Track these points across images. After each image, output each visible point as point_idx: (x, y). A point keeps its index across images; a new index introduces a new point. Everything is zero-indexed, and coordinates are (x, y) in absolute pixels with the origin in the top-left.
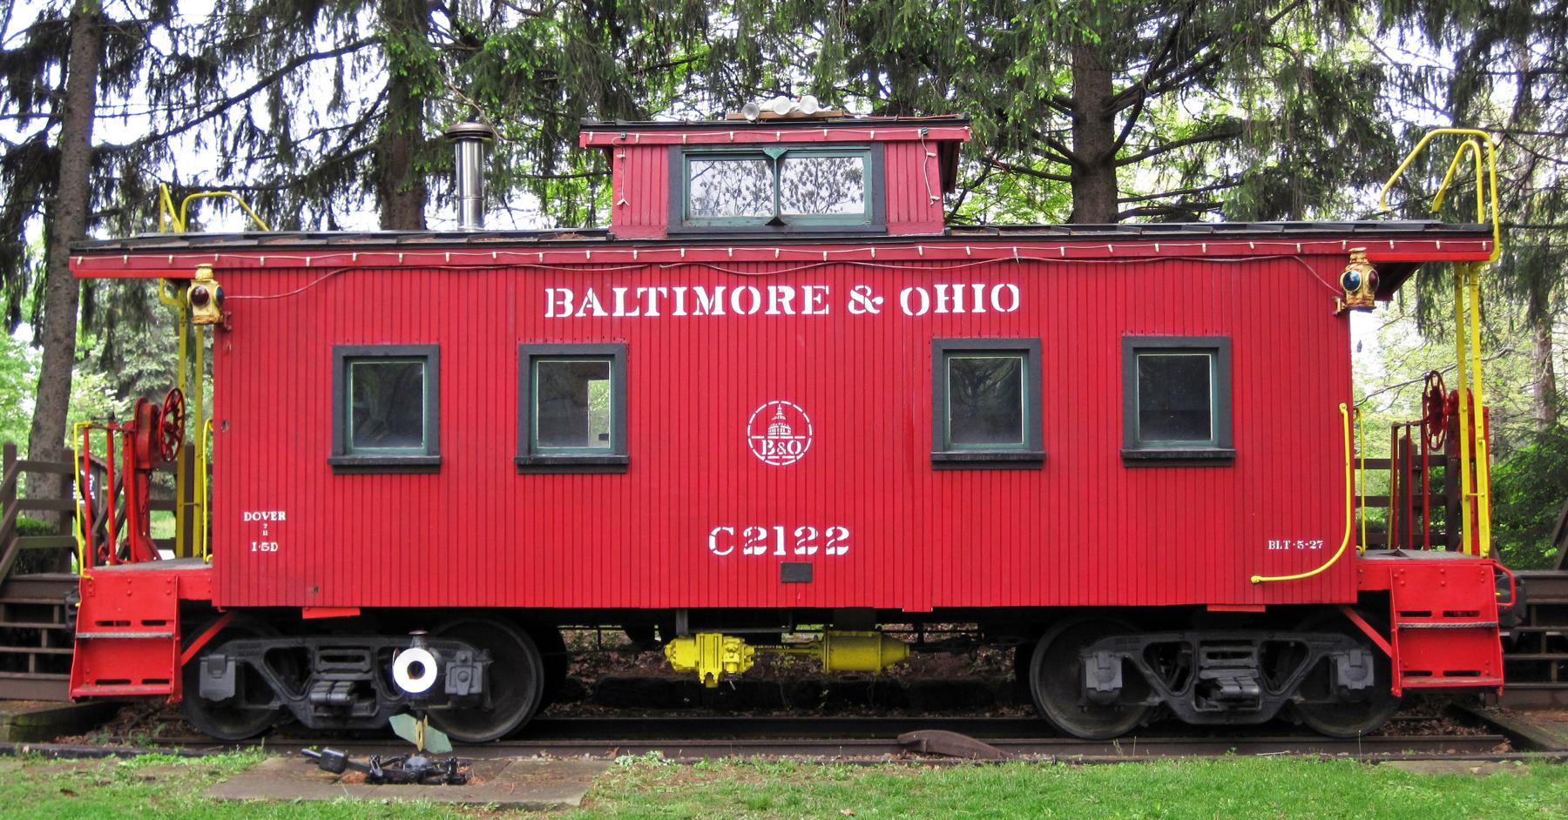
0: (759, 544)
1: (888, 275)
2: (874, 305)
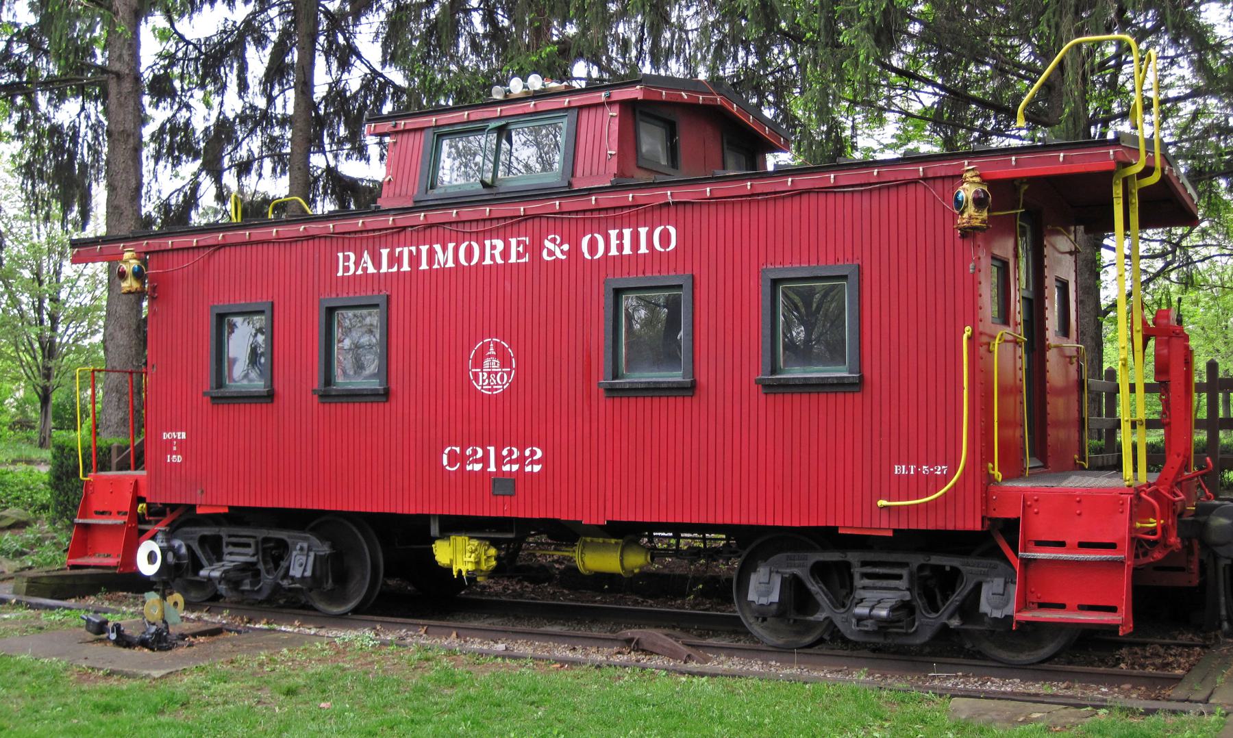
0: (476, 461)
1: (573, 223)
2: (562, 251)
